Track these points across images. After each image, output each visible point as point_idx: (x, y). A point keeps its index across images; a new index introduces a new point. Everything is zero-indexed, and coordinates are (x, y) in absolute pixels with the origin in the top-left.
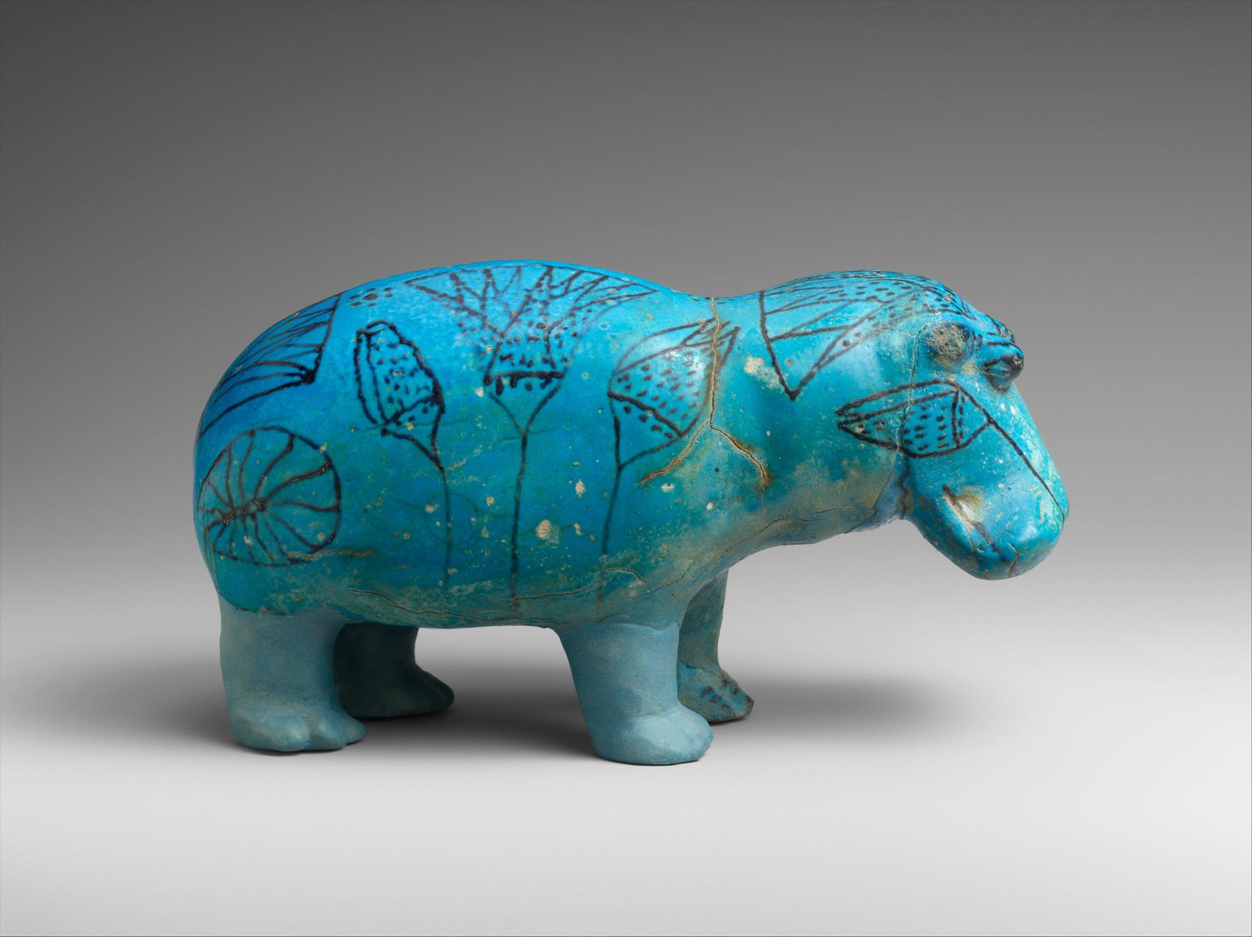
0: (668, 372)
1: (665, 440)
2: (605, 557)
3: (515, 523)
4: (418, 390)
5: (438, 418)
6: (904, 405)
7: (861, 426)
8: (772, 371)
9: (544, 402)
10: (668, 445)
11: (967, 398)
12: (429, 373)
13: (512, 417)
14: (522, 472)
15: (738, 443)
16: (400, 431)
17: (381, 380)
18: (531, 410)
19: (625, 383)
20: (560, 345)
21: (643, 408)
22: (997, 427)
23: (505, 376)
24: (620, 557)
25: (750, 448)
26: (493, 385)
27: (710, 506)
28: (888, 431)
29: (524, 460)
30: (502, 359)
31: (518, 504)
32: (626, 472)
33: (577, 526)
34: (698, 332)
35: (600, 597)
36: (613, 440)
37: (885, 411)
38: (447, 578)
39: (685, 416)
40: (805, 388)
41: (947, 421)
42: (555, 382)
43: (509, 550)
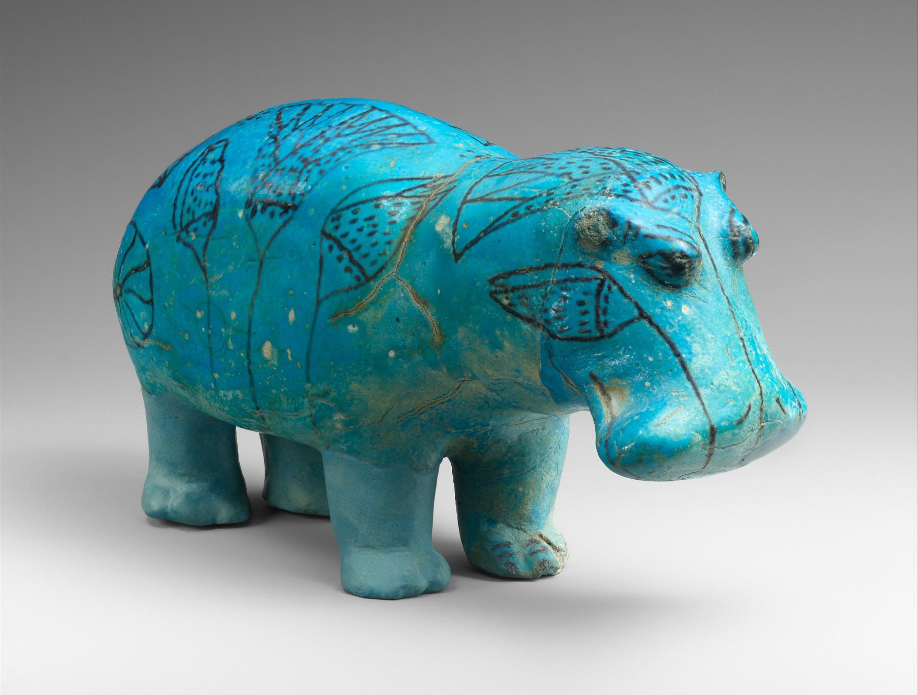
0: (371, 218)
1: (355, 282)
2: (309, 385)
4: (206, 204)
6: (546, 283)
7: (507, 298)
8: (449, 231)
10: (356, 288)
13: (256, 240)
14: (255, 293)
15: (417, 296)
16: (188, 240)
17: (190, 191)
18: (268, 237)
19: (335, 223)
21: (342, 248)
22: (651, 322)
24: (322, 387)
25: (424, 303)
26: (250, 209)
27: (392, 354)
28: (530, 306)
29: (258, 283)
31: (250, 322)
33: (289, 351)
34: (423, 186)
36: (317, 276)
37: (530, 287)
38: (215, 382)
39: (374, 263)
40: (467, 252)
41: (590, 306)
43: (245, 364)
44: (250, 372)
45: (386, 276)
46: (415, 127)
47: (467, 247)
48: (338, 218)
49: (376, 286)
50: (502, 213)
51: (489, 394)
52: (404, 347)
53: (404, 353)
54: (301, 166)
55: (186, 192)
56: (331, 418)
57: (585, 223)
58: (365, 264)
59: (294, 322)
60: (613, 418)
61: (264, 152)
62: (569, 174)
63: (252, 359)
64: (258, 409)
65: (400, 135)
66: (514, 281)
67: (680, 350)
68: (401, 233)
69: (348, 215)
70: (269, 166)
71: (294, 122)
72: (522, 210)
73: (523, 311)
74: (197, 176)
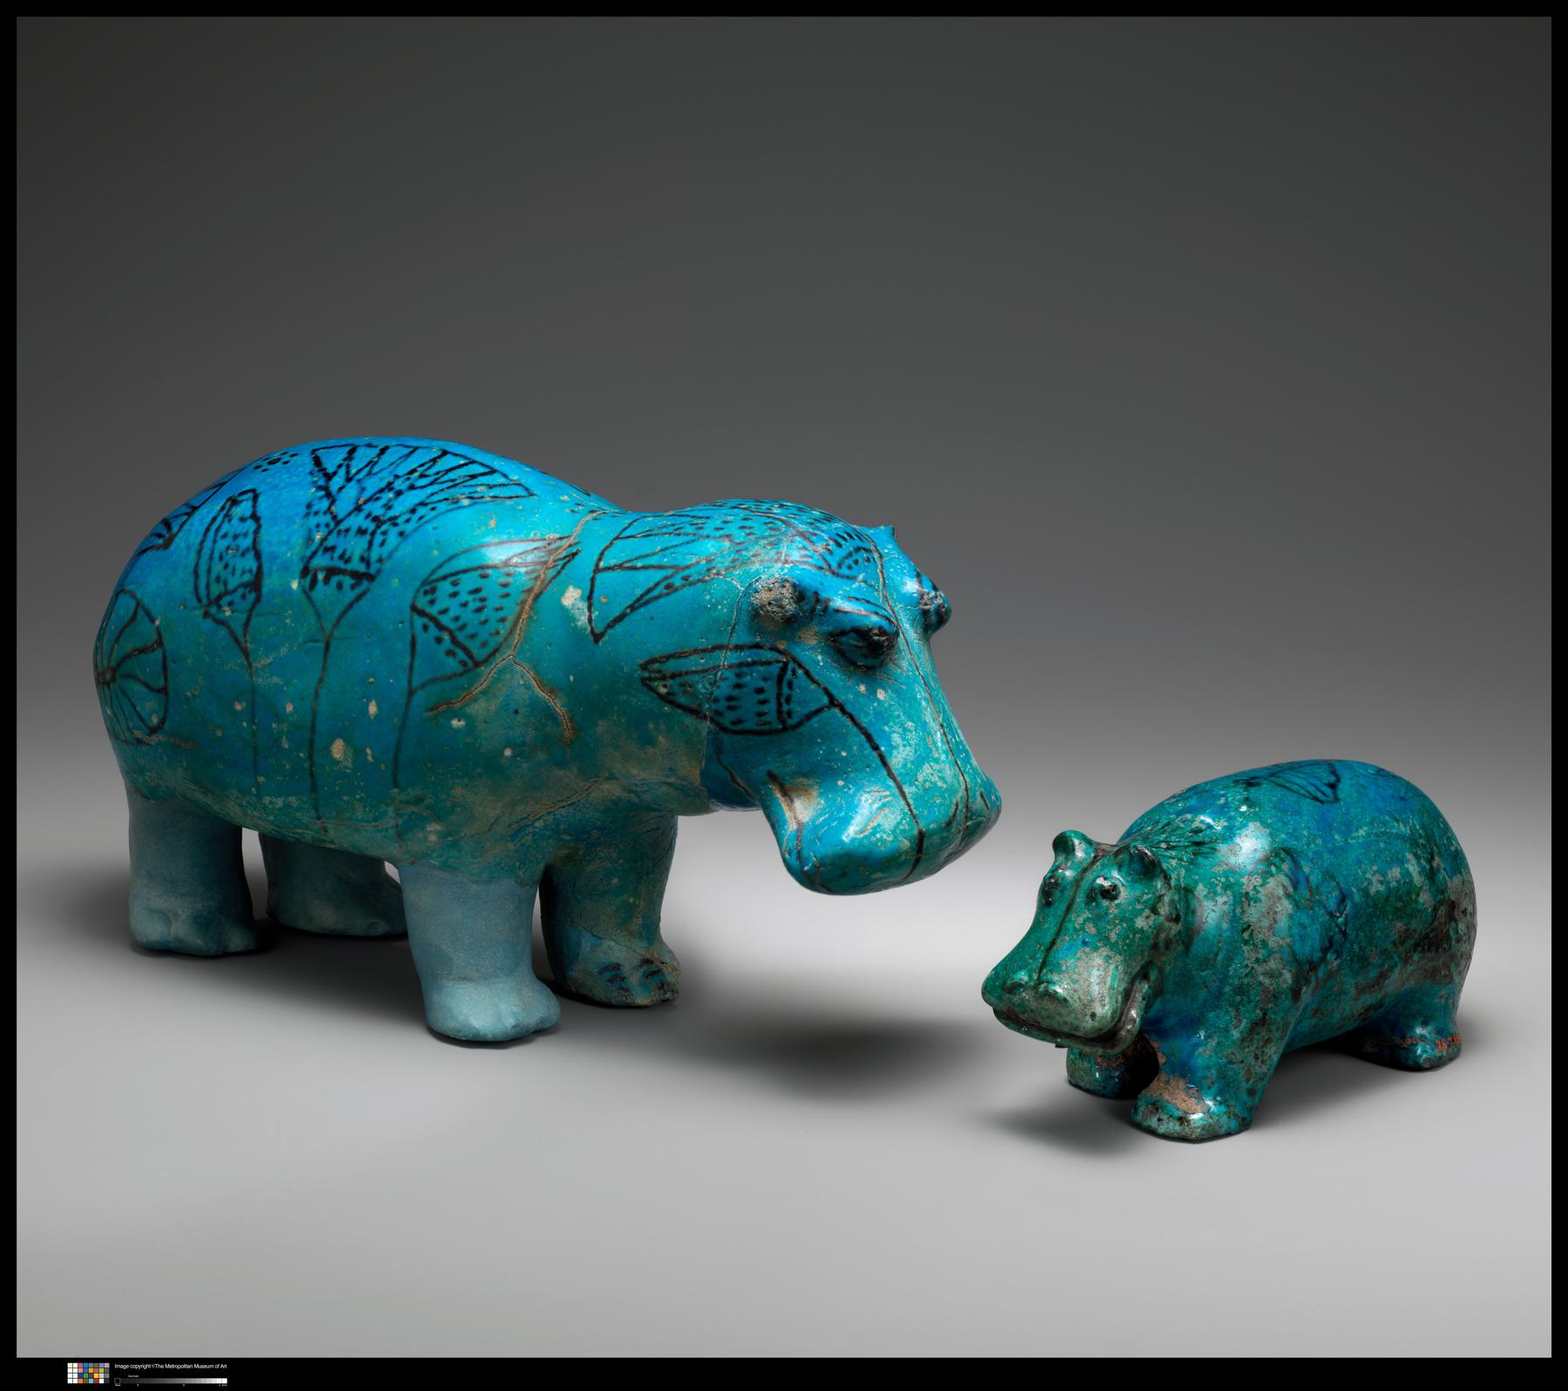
0: (477, 591)
1: (460, 668)
3: (311, 739)
4: (243, 572)
5: (253, 606)
8: (583, 606)
9: (351, 606)
10: (461, 675)
11: (800, 672)
12: (258, 556)
13: (318, 616)
14: (321, 680)
16: (220, 616)
17: (216, 555)
18: (337, 613)
19: (429, 597)
20: (383, 544)
21: (441, 627)
22: (843, 711)
23: (322, 569)
24: (413, 793)
26: (309, 578)
27: (508, 752)
28: (694, 695)
29: (324, 668)
30: (326, 550)
31: (314, 715)
32: (419, 697)
33: (369, 751)
35: (399, 835)
36: (408, 660)
38: (258, 787)
39: (484, 644)
40: (610, 632)
41: (771, 693)
42: (365, 584)
43: (306, 765)
44: (312, 775)
45: (499, 661)
46: (505, 476)
47: (610, 626)
48: (433, 591)
49: (487, 673)
50: (652, 584)
51: (626, 795)
52: (524, 743)
53: (520, 750)
54: (372, 526)
55: (211, 558)
56: (423, 829)
57: (764, 597)
58: (473, 646)
59: (377, 716)
60: (800, 824)
61: (314, 509)
62: (728, 536)
63: (317, 760)
64: (319, 818)
65: (491, 487)
66: (671, 666)
67: (878, 741)
68: (517, 609)
69: (446, 587)
70: (327, 525)
71: (343, 469)
72: (677, 581)
73: (683, 700)
74: (225, 536)
